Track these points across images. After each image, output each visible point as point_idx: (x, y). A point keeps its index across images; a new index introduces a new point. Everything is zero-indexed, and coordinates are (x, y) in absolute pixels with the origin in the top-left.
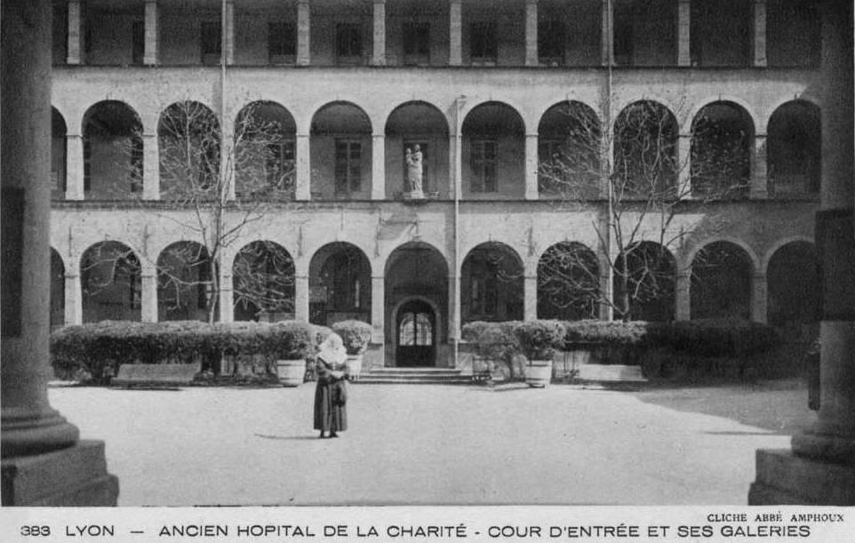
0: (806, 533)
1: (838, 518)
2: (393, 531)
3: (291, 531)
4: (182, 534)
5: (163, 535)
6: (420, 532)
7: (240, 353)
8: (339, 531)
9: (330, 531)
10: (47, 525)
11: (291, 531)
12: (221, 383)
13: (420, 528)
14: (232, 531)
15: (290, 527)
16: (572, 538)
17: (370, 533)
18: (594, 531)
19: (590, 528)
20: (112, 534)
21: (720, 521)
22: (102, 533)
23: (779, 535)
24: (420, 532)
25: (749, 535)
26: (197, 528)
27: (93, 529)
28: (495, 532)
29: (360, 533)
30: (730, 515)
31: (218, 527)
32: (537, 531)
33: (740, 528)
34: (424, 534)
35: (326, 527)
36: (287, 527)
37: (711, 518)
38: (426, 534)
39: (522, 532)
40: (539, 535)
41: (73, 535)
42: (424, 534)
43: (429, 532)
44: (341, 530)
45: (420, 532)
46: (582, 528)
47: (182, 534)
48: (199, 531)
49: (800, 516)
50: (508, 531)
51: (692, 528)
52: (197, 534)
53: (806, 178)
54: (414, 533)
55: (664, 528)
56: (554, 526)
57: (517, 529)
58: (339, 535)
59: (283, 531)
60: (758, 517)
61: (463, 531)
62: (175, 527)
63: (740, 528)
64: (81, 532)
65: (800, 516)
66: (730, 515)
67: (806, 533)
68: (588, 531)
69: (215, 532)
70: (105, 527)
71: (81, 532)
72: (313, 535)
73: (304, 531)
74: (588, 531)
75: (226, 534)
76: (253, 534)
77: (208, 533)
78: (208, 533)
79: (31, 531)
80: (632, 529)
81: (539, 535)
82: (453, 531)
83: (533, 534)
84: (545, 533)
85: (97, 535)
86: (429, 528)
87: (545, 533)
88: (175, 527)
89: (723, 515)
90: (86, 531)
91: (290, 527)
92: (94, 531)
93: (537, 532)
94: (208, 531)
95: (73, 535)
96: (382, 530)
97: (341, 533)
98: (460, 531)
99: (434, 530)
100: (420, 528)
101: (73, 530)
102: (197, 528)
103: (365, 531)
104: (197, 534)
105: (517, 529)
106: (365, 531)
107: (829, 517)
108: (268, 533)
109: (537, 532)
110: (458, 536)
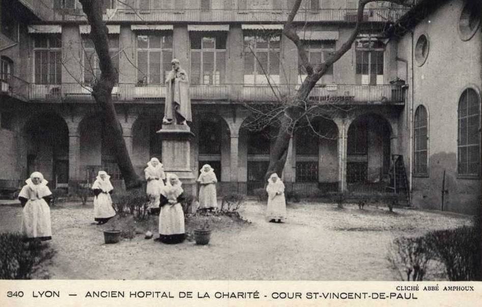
0: (310, 297)
1: (470, 289)
2: (218, 295)
3: (160, 295)
4: (338, 298)
5: (232, 298)
6: (233, 296)
7: (107, 159)
8: (380, 296)
9: (182, 295)
10: (11, 291)
11: (160, 295)
12: (358, 59)
13: (233, 293)
14: (127, 295)
15: (160, 292)
16: (113, 298)
17: (205, 296)
18: (363, 296)
19: (94, 296)
20: (123, 296)
21: (156, 292)
22: (340, 294)
23: (243, 297)
24: (164, 295)
25: (170, 297)
26: (107, 293)
27: (103, 293)
28: (275, 296)
29: (414, 297)
30: (399, 287)
31: (119, 292)
32: (299, 295)
33: (400, 294)
34: (235, 297)
35: (180, 293)
36: (158, 293)
37: (398, 288)
38: (237, 297)
39: (291, 296)
40: (301, 298)
41: (37, 297)
42: (235, 297)
43: (238, 295)
44: (188, 295)
45: (233, 295)
46: (356, 294)
47: (338, 298)
48: (108, 294)
49: (449, 287)
50: (283, 295)
51: (349, 294)
52: (107, 296)
53: (299, 98)
54: (230, 296)
55: (365, 293)
56: (182, 291)
57: (288, 294)
58: (188, 297)
59: (155, 295)
60: (445, 288)
61: (190, 295)
62: (94, 292)
63: (400, 294)
64: (41, 295)
65: (449, 287)
66: (399, 287)
67: (310, 297)
68: (122, 294)
69: (117, 295)
70: (54, 292)
71: (41, 295)
72: (417, 298)
73: (168, 295)
74: (122, 294)
75: (58, 296)
76: (139, 296)
77: (113, 295)
78: (113, 295)
79: (10, 294)
80: (350, 295)
81: (301, 298)
82: (252, 295)
83: (132, 296)
84: (304, 296)
85: (376, 298)
86: (391, 294)
87: (304, 296)
88: (94, 292)
89: (405, 287)
90: (44, 295)
91: (160, 292)
92: (49, 294)
93: (299, 296)
94: (113, 294)
95: (37, 297)
96: (211, 294)
97: (189, 296)
98: (256, 295)
99: (241, 295)
100: (233, 293)
101: (36, 294)
102: (107, 293)
103: (202, 295)
104: (107, 296)
105: (288, 294)
106: (202, 295)
107: (465, 288)
108: (148, 296)
109: (299, 296)
110: (254, 297)
